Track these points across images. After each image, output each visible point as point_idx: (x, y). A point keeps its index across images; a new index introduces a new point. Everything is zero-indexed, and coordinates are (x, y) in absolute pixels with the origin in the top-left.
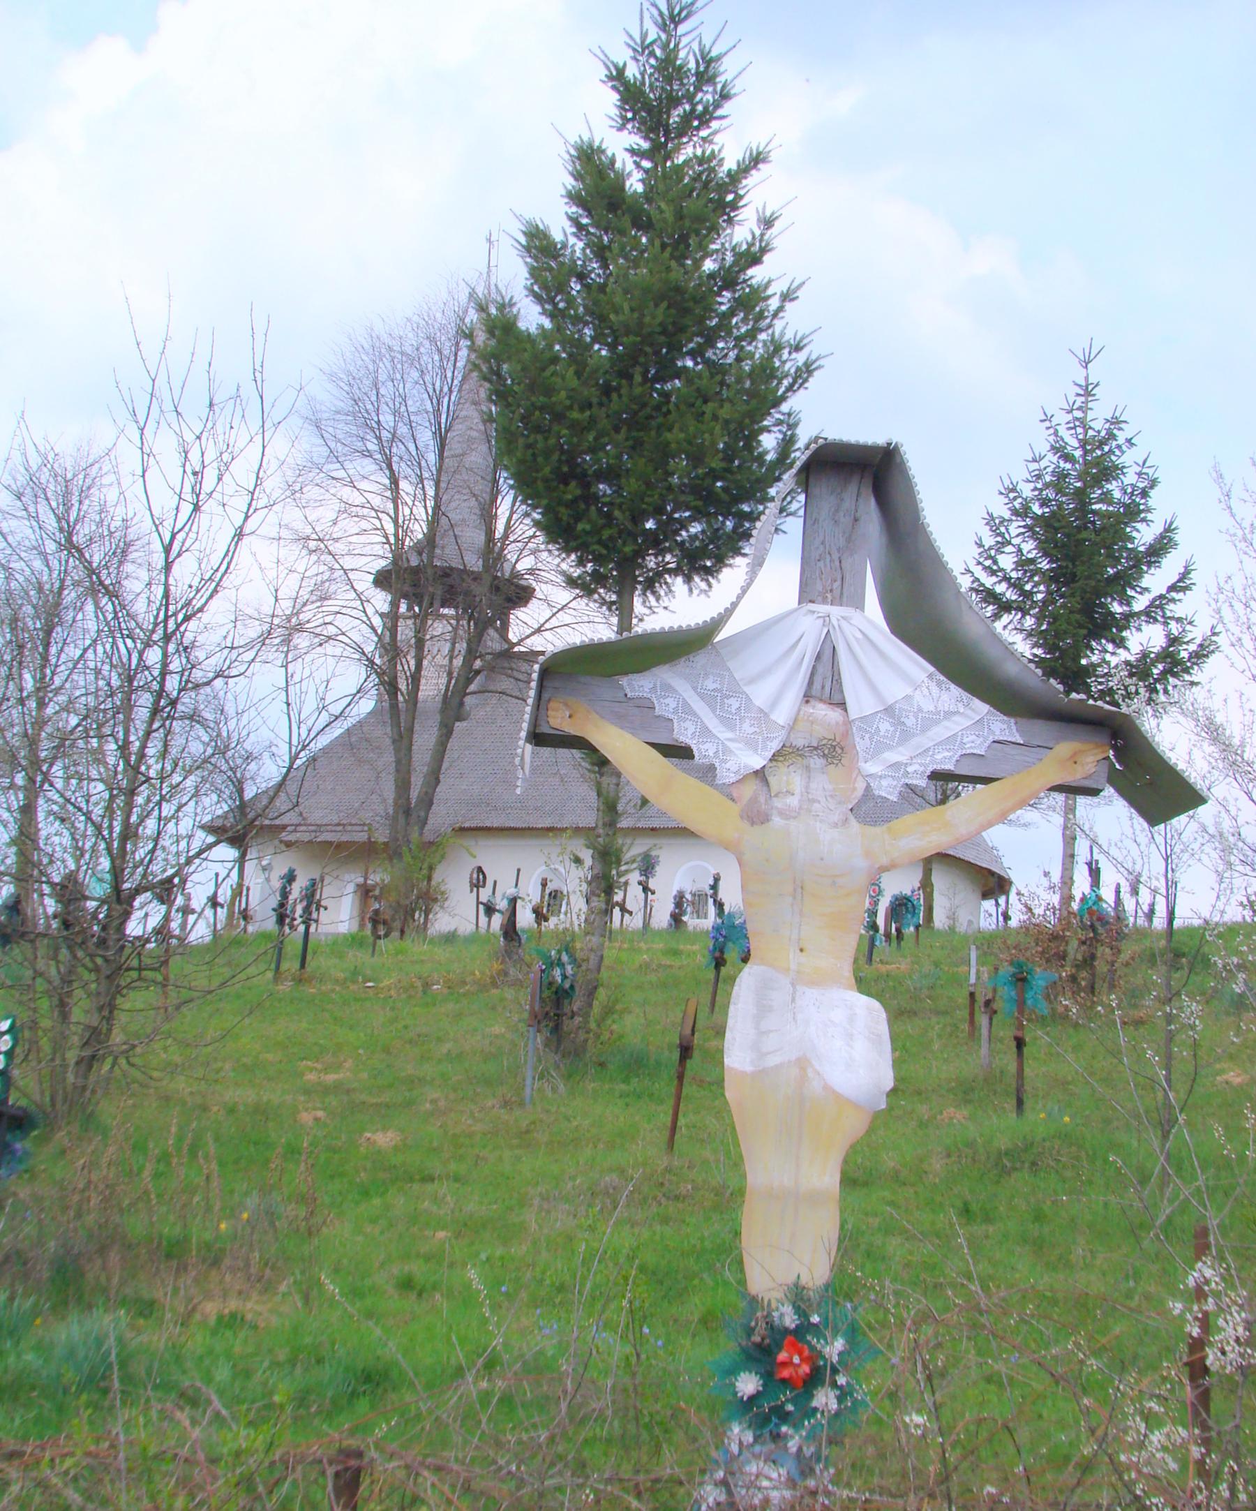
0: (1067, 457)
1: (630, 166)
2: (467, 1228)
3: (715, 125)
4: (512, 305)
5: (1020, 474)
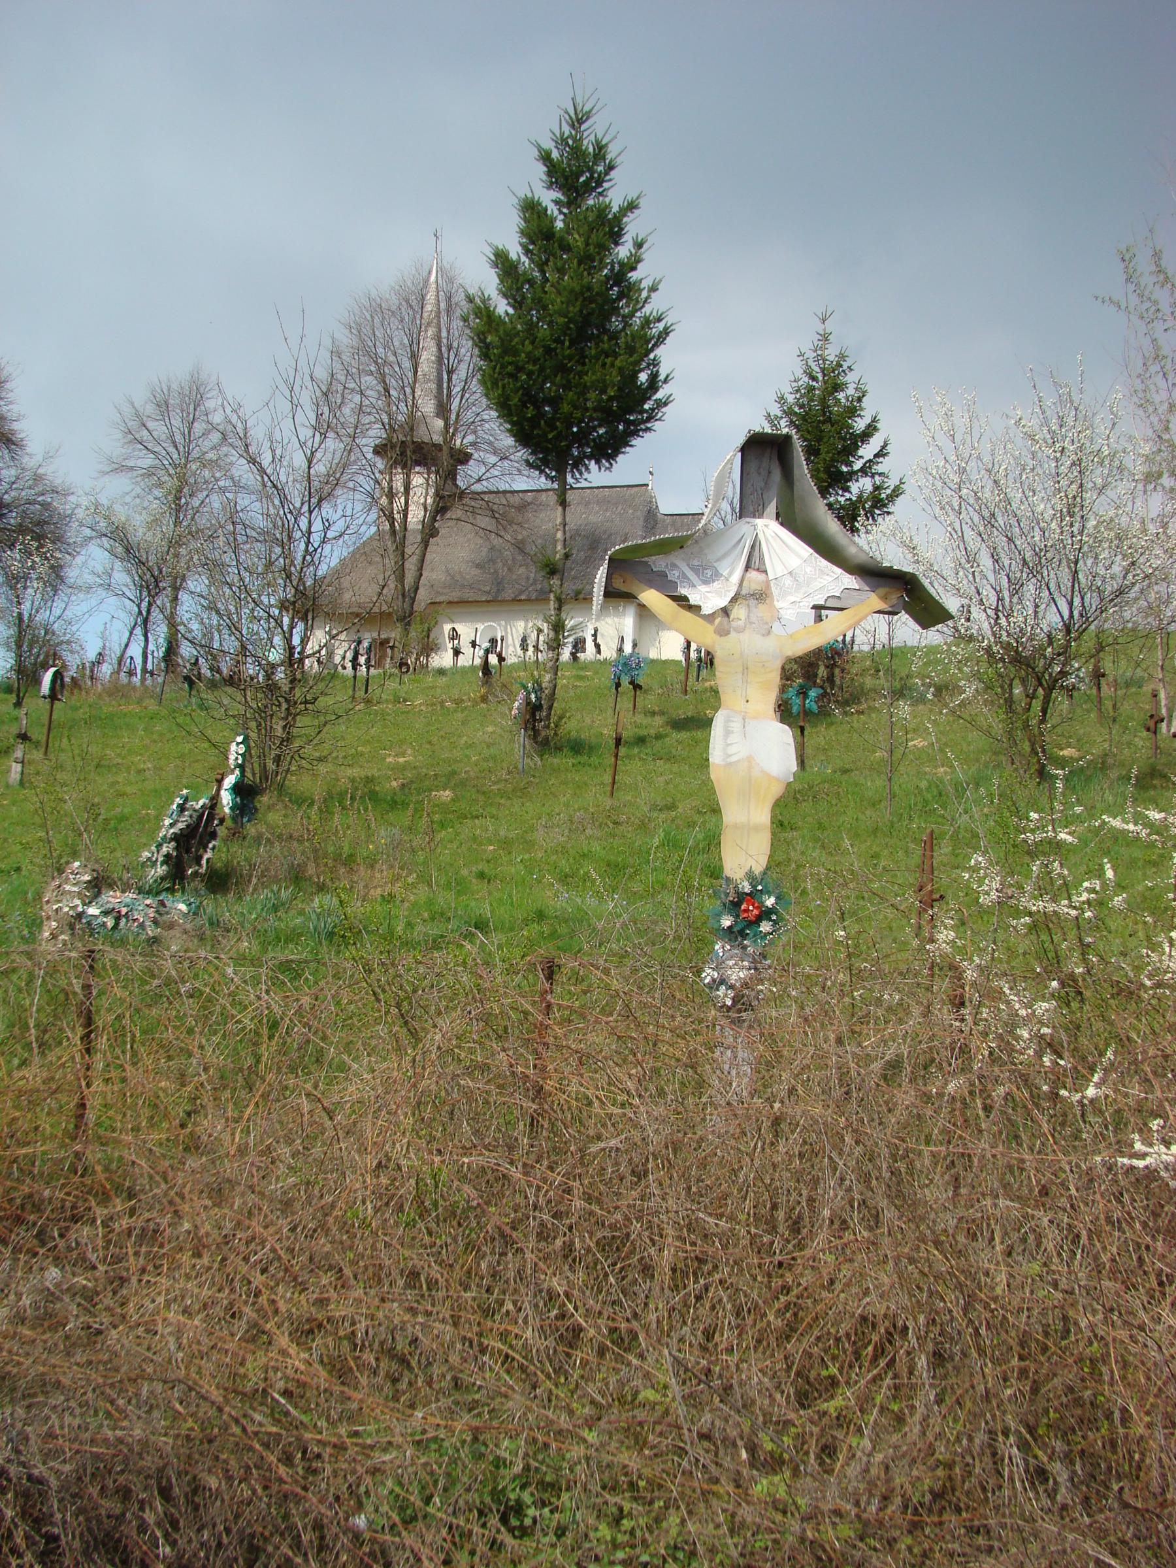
0: (814, 379)
1: (556, 212)
2: (506, 844)
3: (606, 185)
4: (489, 299)
5: (786, 388)
